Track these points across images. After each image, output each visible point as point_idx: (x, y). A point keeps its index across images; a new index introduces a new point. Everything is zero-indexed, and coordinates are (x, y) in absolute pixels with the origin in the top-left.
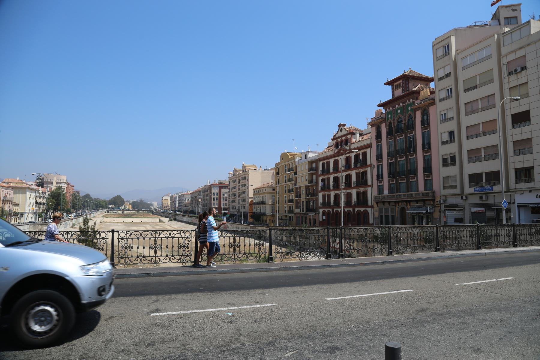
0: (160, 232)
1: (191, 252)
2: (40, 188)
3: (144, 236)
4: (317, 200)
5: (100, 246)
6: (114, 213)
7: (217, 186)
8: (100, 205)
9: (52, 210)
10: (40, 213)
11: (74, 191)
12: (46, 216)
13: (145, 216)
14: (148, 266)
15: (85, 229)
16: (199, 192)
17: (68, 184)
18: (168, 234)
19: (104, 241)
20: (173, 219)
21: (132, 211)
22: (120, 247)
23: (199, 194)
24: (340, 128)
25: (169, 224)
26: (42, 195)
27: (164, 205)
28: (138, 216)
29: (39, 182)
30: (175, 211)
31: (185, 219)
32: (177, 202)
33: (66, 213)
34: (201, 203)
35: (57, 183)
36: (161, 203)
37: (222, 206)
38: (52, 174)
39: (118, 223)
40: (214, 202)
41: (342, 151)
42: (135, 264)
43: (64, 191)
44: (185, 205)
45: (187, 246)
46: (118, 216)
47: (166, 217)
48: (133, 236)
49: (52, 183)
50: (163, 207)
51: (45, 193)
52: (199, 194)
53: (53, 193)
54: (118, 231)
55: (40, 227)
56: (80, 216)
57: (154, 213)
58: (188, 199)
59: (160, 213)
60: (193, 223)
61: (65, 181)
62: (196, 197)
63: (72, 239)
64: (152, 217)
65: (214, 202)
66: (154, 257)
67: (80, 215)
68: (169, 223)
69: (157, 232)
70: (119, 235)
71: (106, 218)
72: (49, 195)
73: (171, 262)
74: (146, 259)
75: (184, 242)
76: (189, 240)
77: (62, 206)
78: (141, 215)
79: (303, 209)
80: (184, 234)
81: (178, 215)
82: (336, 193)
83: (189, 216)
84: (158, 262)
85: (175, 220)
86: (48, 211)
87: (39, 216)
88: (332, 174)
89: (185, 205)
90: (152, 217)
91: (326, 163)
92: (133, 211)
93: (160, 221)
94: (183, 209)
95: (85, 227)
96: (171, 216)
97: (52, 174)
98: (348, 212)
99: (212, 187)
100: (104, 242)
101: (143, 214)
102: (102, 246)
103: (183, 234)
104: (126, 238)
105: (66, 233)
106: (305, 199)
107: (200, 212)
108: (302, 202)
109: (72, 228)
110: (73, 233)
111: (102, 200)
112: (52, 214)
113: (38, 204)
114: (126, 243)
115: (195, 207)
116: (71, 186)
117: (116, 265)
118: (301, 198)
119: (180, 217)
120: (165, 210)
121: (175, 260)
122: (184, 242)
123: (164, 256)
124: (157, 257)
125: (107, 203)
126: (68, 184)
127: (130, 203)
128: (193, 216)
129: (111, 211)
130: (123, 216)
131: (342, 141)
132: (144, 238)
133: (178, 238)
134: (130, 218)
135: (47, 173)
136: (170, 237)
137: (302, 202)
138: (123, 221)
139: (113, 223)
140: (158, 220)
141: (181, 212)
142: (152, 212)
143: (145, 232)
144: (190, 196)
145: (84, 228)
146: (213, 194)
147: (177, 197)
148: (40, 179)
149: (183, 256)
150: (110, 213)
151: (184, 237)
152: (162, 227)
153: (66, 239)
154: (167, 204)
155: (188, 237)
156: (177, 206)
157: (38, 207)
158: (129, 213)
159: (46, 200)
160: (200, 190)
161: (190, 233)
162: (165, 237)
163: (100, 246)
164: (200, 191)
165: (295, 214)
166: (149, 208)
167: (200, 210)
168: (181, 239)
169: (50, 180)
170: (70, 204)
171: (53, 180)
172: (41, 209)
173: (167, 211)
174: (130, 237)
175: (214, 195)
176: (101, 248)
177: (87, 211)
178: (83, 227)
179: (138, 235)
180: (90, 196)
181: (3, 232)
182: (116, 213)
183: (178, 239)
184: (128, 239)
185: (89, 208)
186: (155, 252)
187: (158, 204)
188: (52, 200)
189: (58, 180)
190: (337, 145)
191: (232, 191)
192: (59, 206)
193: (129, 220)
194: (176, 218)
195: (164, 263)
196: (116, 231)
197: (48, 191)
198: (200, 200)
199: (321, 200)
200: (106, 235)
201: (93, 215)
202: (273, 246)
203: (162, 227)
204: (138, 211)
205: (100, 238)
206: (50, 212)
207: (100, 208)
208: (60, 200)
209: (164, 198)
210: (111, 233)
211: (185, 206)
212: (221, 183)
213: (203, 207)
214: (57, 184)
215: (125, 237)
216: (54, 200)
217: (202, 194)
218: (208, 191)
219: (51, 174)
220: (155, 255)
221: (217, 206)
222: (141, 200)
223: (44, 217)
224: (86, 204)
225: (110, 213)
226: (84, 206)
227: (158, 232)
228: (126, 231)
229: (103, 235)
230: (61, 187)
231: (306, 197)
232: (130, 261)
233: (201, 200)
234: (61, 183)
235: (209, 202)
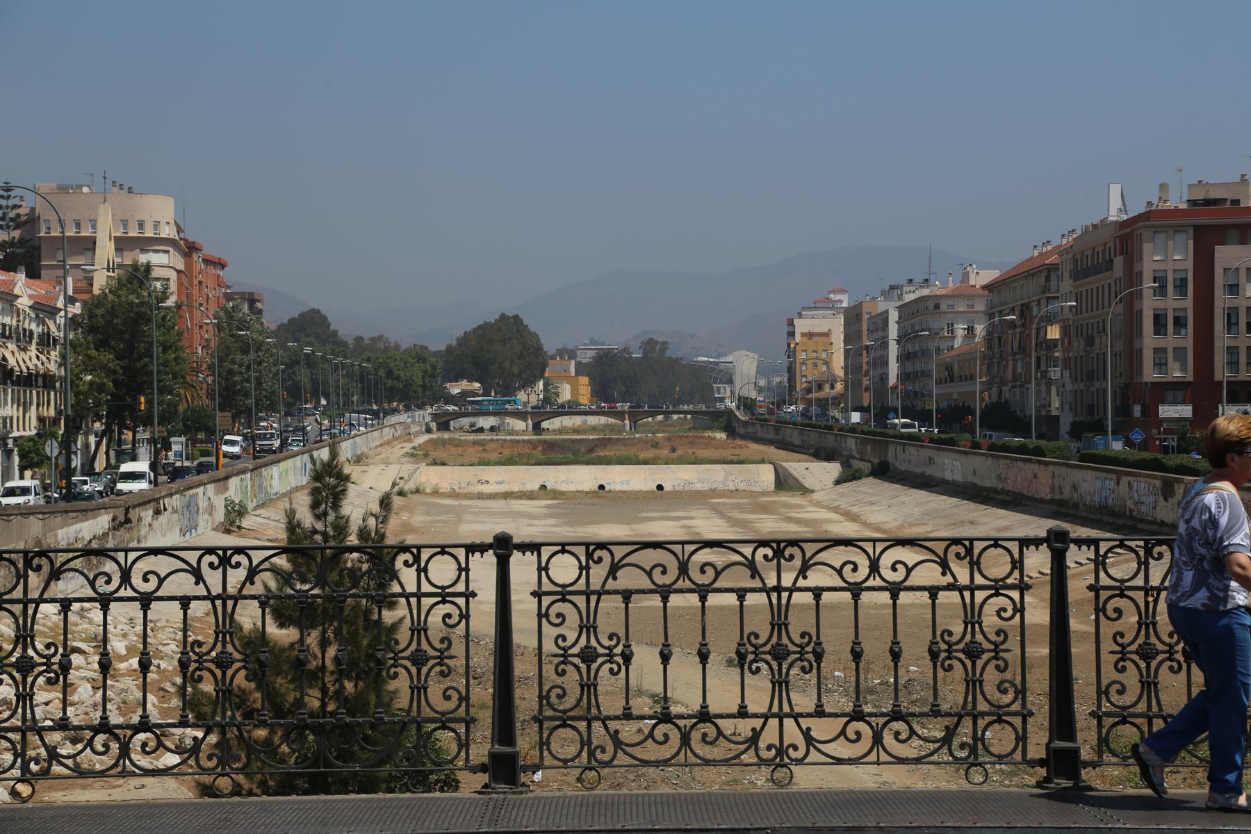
0: (810, 549)
2: (21, 277)
3: (891, 576)
5: (425, 646)
6: (481, 430)
7: (1178, 229)
8: (390, 383)
9: (99, 418)
10: (30, 439)
11: (229, 297)
12: (69, 461)
13: (680, 452)
14: (712, 781)
15: (318, 538)
16: (1048, 279)
17: (189, 249)
19: (447, 608)
20: (866, 467)
21: (593, 420)
22: (549, 646)
23: (1046, 289)
25: (843, 503)
26: (33, 326)
27: (807, 374)
28: (632, 451)
29: (12, 244)
30: (883, 413)
31: (953, 466)
32: (893, 350)
33: (183, 439)
34: (1065, 350)
35: (122, 244)
36: (783, 361)
37: (1222, 373)
38: (85, 190)
39: (507, 495)
40: (1160, 342)
42: (646, 763)
43: (164, 296)
44: (949, 368)
45: (996, 651)
46: (507, 452)
47: (823, 454)
48: (628, 579)
49: (89, 245)
50: (801, 385)
51: (53, 312)
52: (1046, 289)
53: (99, 312)
54: (535, 547)
55: (35, 526)
56: (271, 457)
57: (742, 431)
58: (970, 330)
59: (777, 429)
60: (1007, 493)
61: (167, 232)
62: (1025, 311)
63: (616, 592)
64: (726, 453)
65: (1160, 342)
66: (774, 722)
67: (270, 451)
68: (842, 495)
69: (36, 561)
70: (540, 569)
71: (435, 464)
72: (73, 322)
73: (884, 757)
75: (972, 617)
76: (455, 612)
77: (162, 391)
78: (656, 445)
80: (419, 571)
81: (902, 436)
83: (976, 445)
84: (799, 754)
85: (883, 472)
86: (74, 426)
87: (22, 457)
89: (949, 368)
90: (726, 453)
92: (602, 420)
93: (784, 482)
94: (936, 395)
95: (319, 526)
96: (851, 444)
97: (85, 190)
99: (1146, 234)
100: (449, 616)
101: (669, 439)
102: (438, 646)
103: (962, 574)
104: (587, 594)
105: (216, 561)
107: (1054, 413)
109: (228, 531)
111: (404, 347)
112: (98, 444)
113: (13, 384)
114: (588, 626)
115: (1021, 382)
116: (206, 261)
117: (1086, 764)
119: (913, 450)
120: (814, 410)
121: (911, 749)
122: (972, 617)
123: (835, 715)
124: (789, 723)
125: (434, 367)
126: (189, 249)
127: (578, 364)
128: (1005, 448)
129: (465, 422)
130: (538, 453)
132: (895, 590)
133: (933, 591)
134: (587, 463)
135: (54, 185)
138: (543, 487)
139: (481, 496)
140: (765, 476)
141: (923, 417)
142: (728, 423)
143: (899, 549)
144: (980, 306)
145: (315, 531)
146: (1148, 284)
147: (894, 316)
148: (12, 220)
150: (456, 436)
151: (419, 595)
152: (798, 521)
153: (218, 597)
154: (827, 363)
156: (892, 379)
157: (17, 401)
158: (576, 431)
159: (63, 356)
160: (1054, 259)
161: (1013, 562)
162: (839, 583)
163: (425, 646)
164: (1051, 269)
166: (706, 394)
167: (1056, 403)
168: (199, 609)
169: (78, 225)
170: (205, 378)
171: (94, 227)
172: (33, 412)
173: (824, 414)
174: (611, 585)
175: (1161, 290)
176: (432, 653)
177: (310, 424)
178: (306, 518)
179: (664, 572)
180: (329, 326)
182: (492, 429)
183: (933, 596)
184: (599, 594)
185: (323, 402)
186: (780, 684)
187: (761, 371)
188: (93, 352)
189: (125, 227)
192: (140, 391)
193: (580, 478)
194: (890, 458)
195: (839, 761)
196: (524, 547)
197: (70, 300)
198: (1054, 333)
200: (460, 569)
201: (354, 446)
203: (798, 521)
204: (635, 416)
205: (426, 588)
206: (86, 434)
207: (390, 402)
208: (148, 353)
209: (801, 326)
210: (490, 557)
211: (949, 376)
212: (1209, 202)
213: (1075, 379)
214: (119, 249)
215: (1139, 581)
216: (107, 357)
217: (1067, 285)
218: (1109, 265)
219: (80, 187)
220: (775, 709)
221: (1184, 368)
222: (650, 345)
223: (57, 465)
224: (303, 376)
225: (456, 436)
226: (295, 392)
227: (795, 551)
228: (587, 545)
229: (442, 571)
230: (148, 268)
232: (618, 743)
233: (1065, 331)
234: (145, 244)
235: (1120, 347)
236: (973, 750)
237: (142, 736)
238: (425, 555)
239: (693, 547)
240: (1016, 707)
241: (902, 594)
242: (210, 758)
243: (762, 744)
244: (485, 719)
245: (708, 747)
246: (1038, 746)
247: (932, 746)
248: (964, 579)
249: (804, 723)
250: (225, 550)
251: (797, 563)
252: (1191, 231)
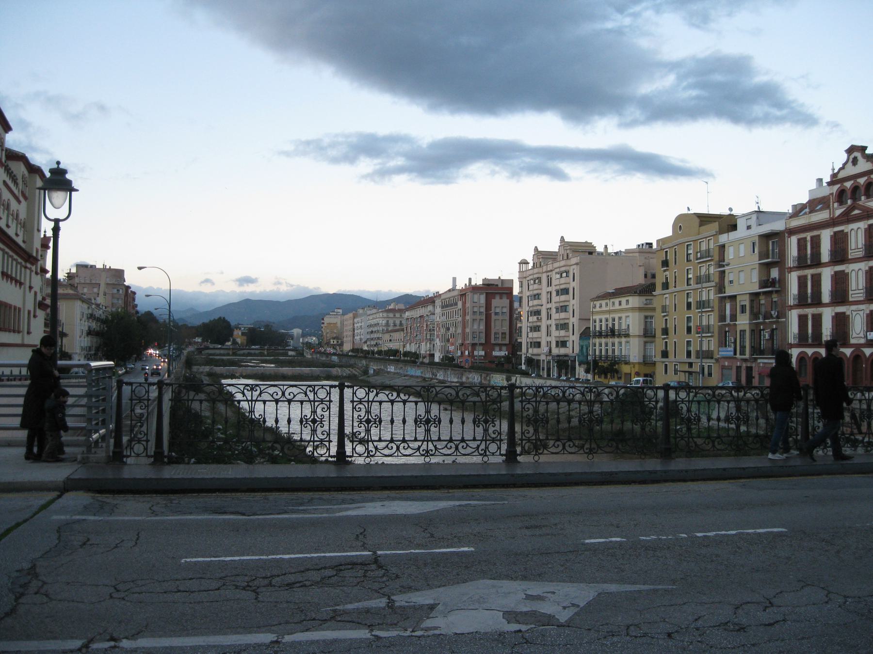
0: (263, 387)
1: (329, 435)
4: (785, 327)
18: (280, 393)
24: (852, 156)
41: (856, 212)
63: (197, 400)
73: (566, 452)
74: (409, 446)
79: (743, 348)
80: (314, 394)
82: (836, 311)
88: (826, 265)
91: (809, 238)
98: (814, 356)
105: (311, 389)
106: (748, 326)
108: (741, 331)
110: (599, 391)
114: (368, 412)
118: (737, 323)
121: (469, 450)
124: (430, 443)
131: (855, 189)
136: (400, 399)
137: (741, 331)
149: (484, 442)
155: (322, 401)
162: (388, 400)
165: (717, 360)
181: (315, 386)
190: (841, 196)
191: (531, 303)
199: (794, 328)
202: (518, 428)
218: (456, 304)
227: (258, 388)
231: (750, 320)
236: (485, 452)
238: (316, 388)
239: (287, 387)
240: (327, 439)
241: (561, 403)
242: (587, 449)
243: (480, 449)
244: (334, 438)
245: (464, 450)
246: (152, 450)
247: (415, 451)
248: (312, 398)
249: (435, 443)
250: (252, 385)
252: (485, 294)
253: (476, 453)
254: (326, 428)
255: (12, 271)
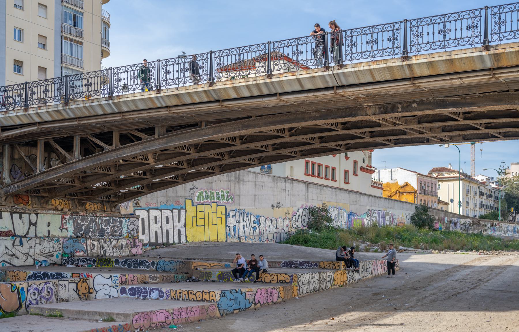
73: (516, 37)
103: (471, 15)
104: (499, 14)
215: (498, 12)
236: (473, 42)
237: (433, 44)
251: (502, 9)
253: (440, 47)
254: (493, 20)
255: (160, 103)
